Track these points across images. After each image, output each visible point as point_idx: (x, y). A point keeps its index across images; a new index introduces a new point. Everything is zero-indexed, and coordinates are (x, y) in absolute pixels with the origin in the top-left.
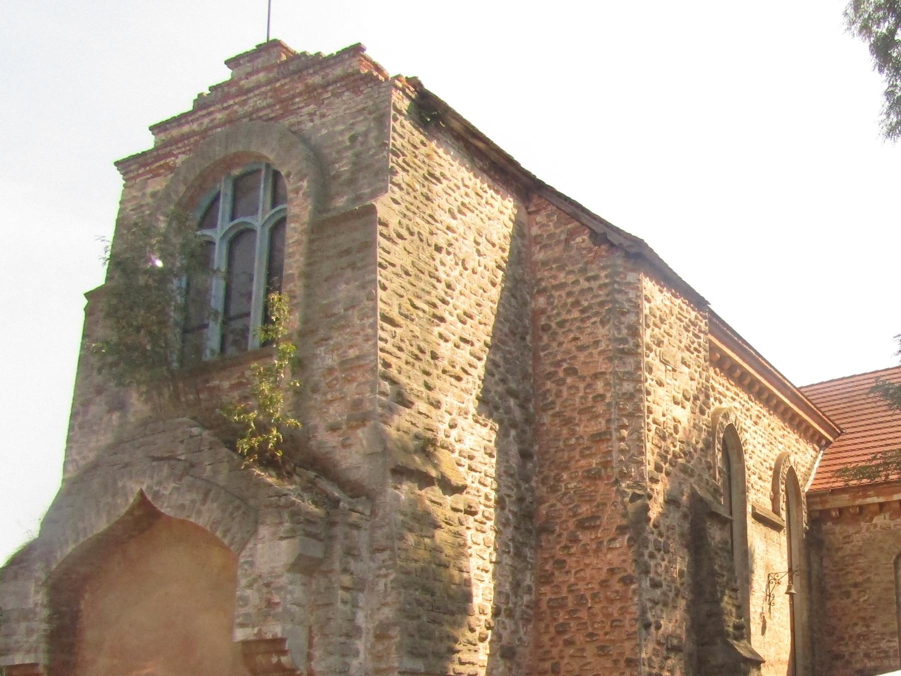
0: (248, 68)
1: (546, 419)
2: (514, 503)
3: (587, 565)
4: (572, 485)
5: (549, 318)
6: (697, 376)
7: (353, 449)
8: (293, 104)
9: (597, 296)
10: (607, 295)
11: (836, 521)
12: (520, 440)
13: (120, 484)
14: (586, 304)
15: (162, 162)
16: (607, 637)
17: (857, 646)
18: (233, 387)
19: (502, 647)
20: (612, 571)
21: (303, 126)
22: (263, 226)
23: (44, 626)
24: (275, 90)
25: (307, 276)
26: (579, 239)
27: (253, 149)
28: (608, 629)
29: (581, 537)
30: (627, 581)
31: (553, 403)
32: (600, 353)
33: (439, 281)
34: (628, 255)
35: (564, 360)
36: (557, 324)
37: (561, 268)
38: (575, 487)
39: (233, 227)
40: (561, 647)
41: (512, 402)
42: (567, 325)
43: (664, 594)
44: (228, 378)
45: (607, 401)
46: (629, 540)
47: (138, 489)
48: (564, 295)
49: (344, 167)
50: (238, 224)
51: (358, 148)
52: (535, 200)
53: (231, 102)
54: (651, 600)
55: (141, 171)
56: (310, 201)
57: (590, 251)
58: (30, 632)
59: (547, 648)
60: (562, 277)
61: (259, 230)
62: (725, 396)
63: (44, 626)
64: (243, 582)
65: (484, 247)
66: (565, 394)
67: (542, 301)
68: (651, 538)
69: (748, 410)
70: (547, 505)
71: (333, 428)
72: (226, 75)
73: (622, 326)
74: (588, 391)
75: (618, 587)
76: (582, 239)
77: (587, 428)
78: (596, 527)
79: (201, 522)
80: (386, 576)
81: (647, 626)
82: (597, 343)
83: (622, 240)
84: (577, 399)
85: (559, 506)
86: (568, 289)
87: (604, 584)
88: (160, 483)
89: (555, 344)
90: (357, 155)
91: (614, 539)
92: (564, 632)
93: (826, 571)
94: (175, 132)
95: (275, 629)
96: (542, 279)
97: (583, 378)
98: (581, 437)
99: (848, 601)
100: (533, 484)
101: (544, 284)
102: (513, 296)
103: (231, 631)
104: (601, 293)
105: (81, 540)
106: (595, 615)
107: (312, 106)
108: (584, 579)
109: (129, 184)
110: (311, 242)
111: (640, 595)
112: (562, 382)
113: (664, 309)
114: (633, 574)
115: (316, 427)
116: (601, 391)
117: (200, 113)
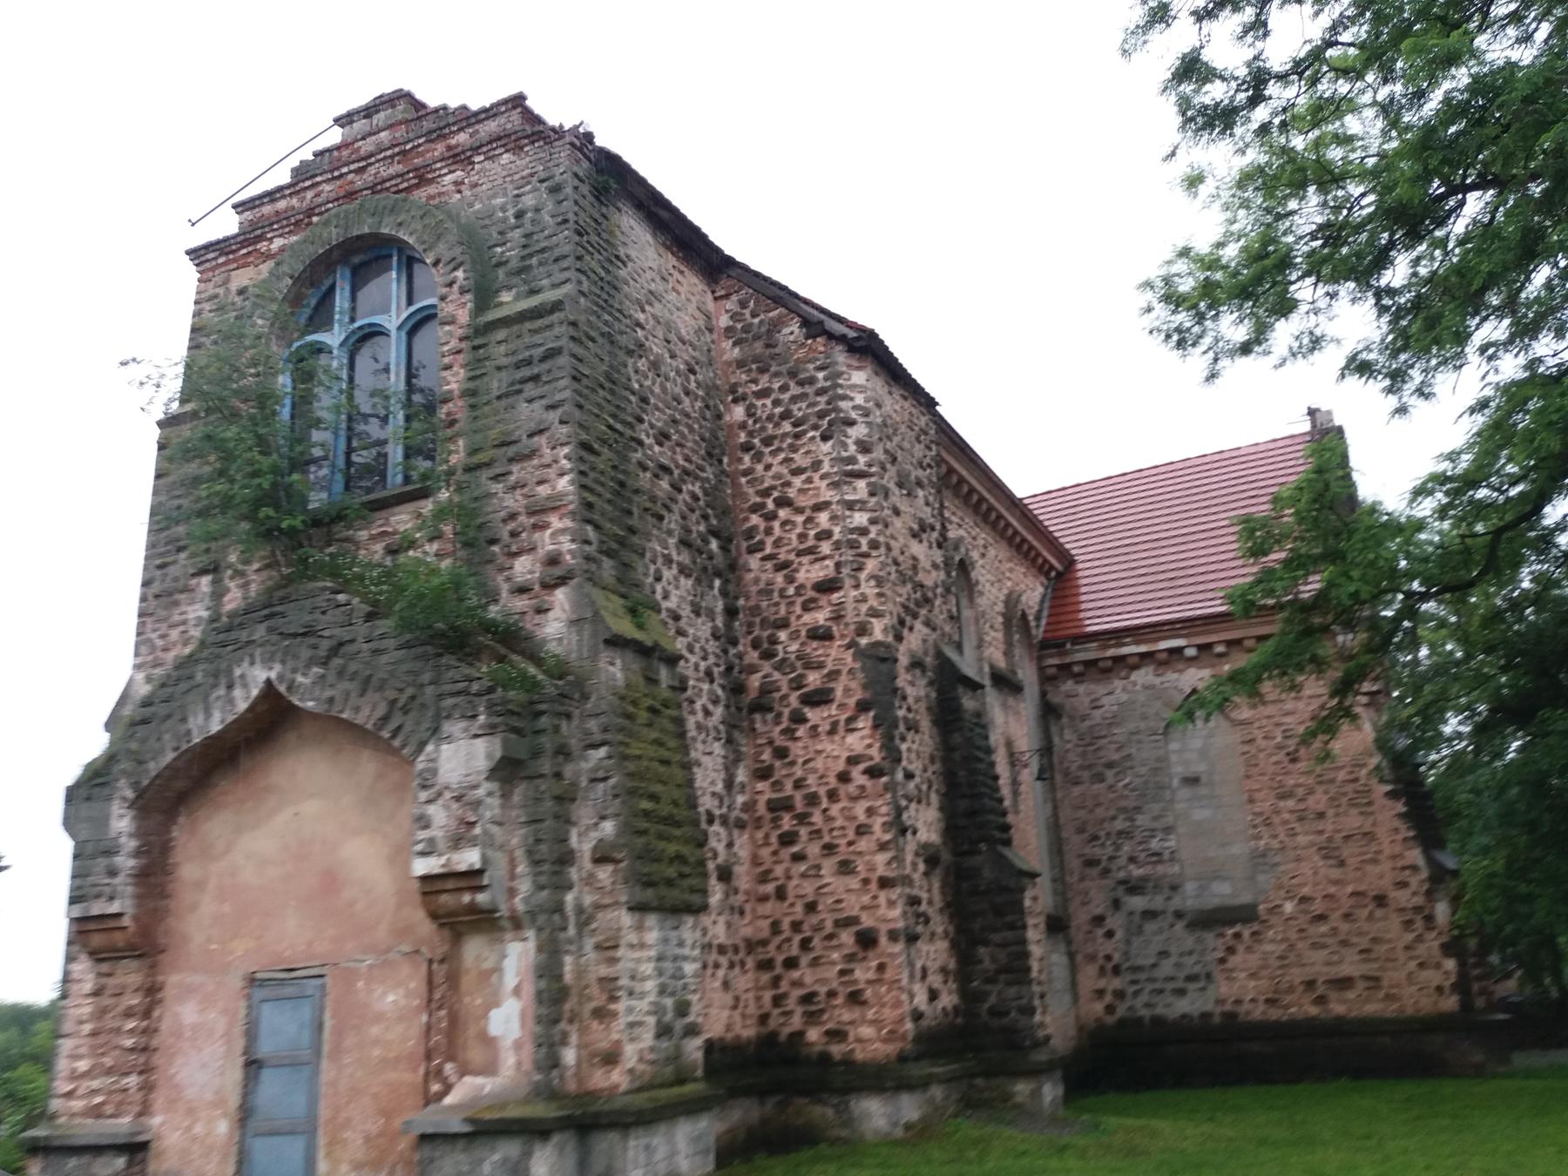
0: (360, 125)
3: (819, 752)
7: (551, 615)
10: (828, 403)
11: (1079, 678)
13: (238, 672)
17: (1118, 847)
23: (132, 862)
26: (786, 331)
28: (851, 835)
37: (762, 371)
39: (353, 332)
42: (776, 444)
43: (918, 787)
46: (875, 718)
50: (360, 328)
51: (528, 227)
53: (345, 170)
61: (393, 333)
63: (132, 862)
65: (678, 348)
66: (777, 531)
67: (739, 412)
70: (760, 675)
71: (522, 590)
72: (335, 136)
73: (849, 441)
76: (792, 330)
77: (811, 573)
78: (829, 701)
82: (817, 465)
84: (794, 537)
85: (776, 675)
86: (773, 396)
87: (844, 777)
89: (760, 467)
94: (267, 209)
95: (470, 858)
97: (800, 511)
100: (740, 648)
106: (832, 819)
107: (459, 173)
111: (894, 791)
117: (302, 185)
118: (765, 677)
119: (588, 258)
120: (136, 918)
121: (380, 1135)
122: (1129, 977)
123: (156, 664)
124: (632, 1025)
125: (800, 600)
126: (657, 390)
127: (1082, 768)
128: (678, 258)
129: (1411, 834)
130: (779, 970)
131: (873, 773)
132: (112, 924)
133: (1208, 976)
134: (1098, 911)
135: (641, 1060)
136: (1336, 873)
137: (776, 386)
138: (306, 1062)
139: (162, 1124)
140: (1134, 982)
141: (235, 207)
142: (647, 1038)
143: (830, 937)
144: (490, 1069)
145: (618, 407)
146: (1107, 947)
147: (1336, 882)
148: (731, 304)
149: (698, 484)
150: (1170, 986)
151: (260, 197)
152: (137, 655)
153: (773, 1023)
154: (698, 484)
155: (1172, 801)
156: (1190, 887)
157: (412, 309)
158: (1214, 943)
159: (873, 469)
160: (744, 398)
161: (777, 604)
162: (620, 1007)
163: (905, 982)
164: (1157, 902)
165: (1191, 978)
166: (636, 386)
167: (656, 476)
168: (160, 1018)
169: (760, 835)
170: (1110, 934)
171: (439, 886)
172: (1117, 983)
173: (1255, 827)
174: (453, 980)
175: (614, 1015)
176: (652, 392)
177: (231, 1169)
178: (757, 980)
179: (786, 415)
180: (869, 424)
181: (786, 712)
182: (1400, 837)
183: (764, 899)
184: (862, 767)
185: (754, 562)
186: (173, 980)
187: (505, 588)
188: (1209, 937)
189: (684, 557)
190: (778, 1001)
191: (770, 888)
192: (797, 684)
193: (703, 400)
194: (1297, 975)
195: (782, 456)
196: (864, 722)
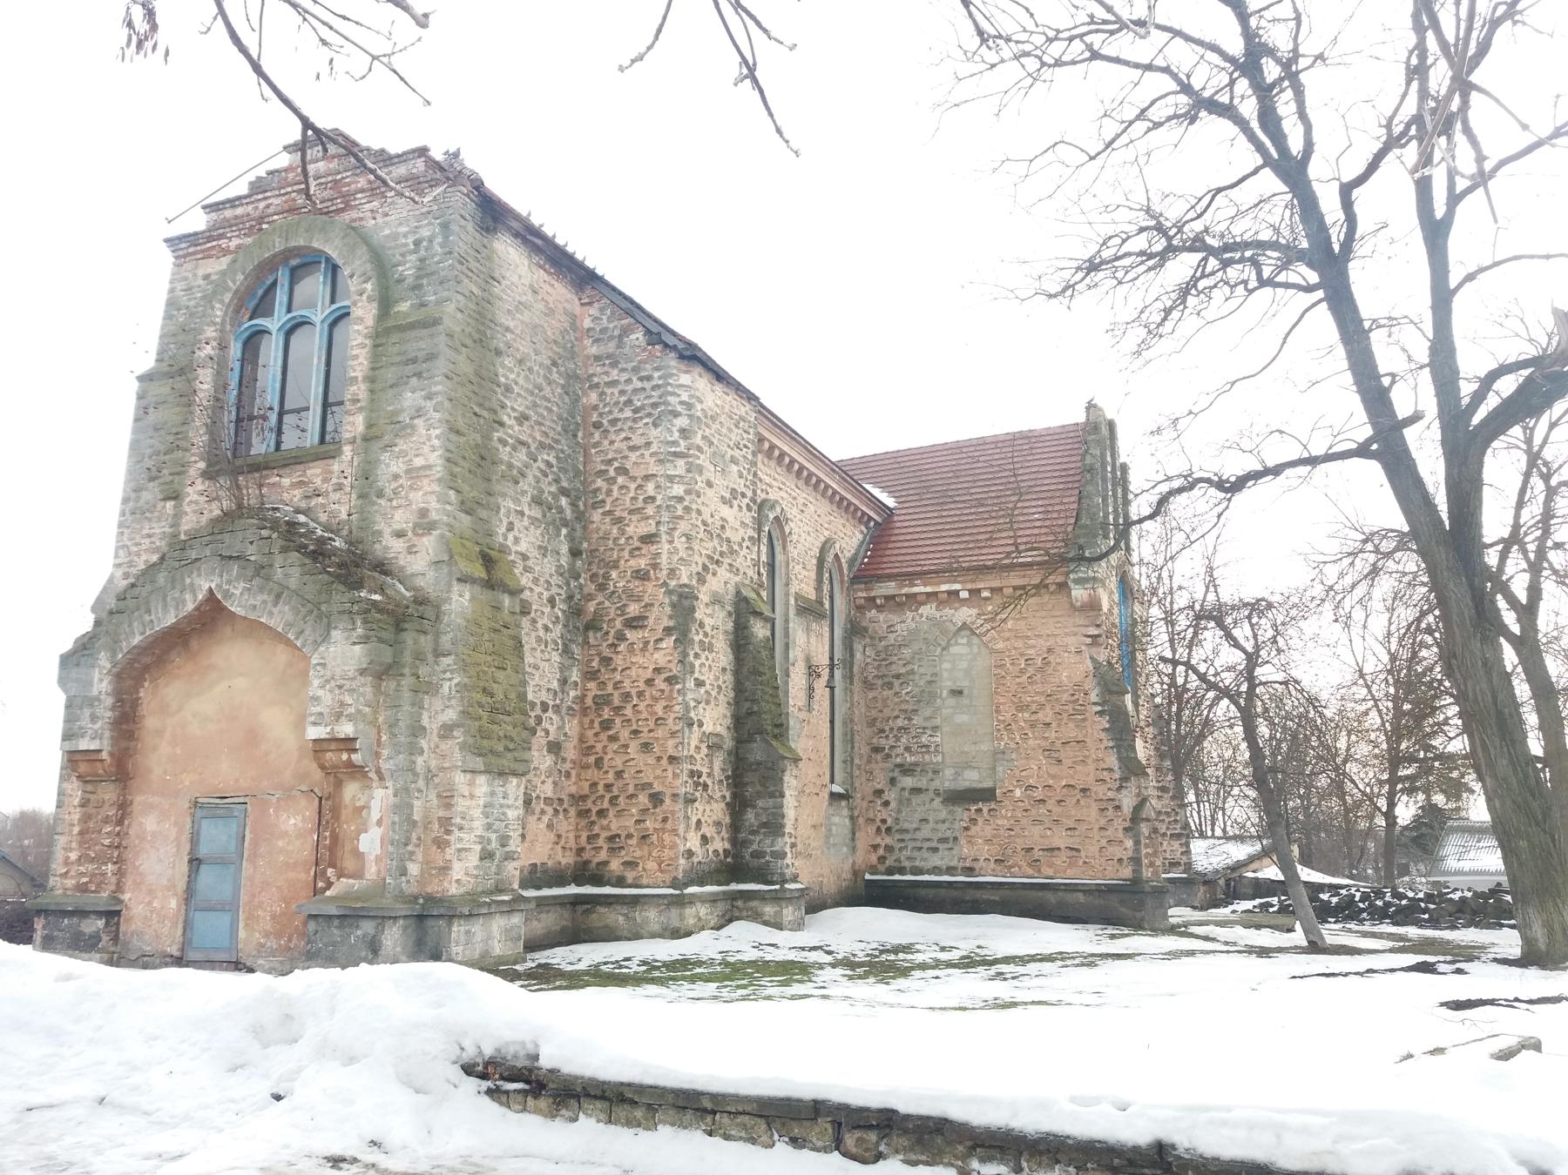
1: (596, 516)
2: (564, 601)
4: (621, 584)
5: (601, 415)
6: (745, 472)
8: (355, 199)
10: (660, 397)
11: (880, 608)
12: (571, 538)
13: (188, 581)
14: (639, 404)
15: (214, 243)
17: (898, 739)
18: (294, 485)
19: (549, 742)
22: (322, 322)
23: (109, 714)
24: (336, 182)
25: (371, 380)
26: (633, 337)
27: (315, 245)
28: (651, 724)
29: (628, 636)
30: (671, 680)
31: (603, 501)
32: (651, 455)
33: (499, 386)
35: (616, 459)
36: (609, 421)
37: (614, 365)
40: (605, 743)
41: (564, 501)
42: (619, 423)
44: (290, 475)
45: (658, 503)
49: (408, 270)
50: (294, 318)
51: (423, 252)
52: (588, 291)
53: (289, 189)
54: (695, 700)
56: (375, 305)
57: (644, 350)
58: (94, 718)
59: (591, 743)
61: (318, 325)
62: (771, 487)
63: (109, 714)
64: (316, 683)
66: (615, 494)
67: (594, 397)
68: (697, 638)
69: (795, 498)
71: (400, 534)
73: (674, 429)
75: (663, 686)
76: (638, 336)
77: (637, 528)
78: (643, 627)
79: (272, 623)
80: (450, 679)
81: (691, 725)
82: (648, 444)
84: (628, 500)
85: (607, 604)
86: (620, 387)
87: (650, 682)
88: (229, 582)
89: (606, 443)
90: (422, 260)
92: (609, 729)
94: (228, 213)
95: (346, 729)
97: (633, 479)
98: (631, 537)
99: (891, 692)
100: (582, 581)
101: (596, 380)
102: (567, 393)
105: (148, 633)
107: (375, 203)
111: (684, 695)
112: (612, 481)
113: (716, 409)
115: (380, 533)
118: (599, 604)
119: (466, 280)
120: (111, 754)
121: (283, 914)
122: (898, 836)
123: (131, 564)
125: (628, 548)
126: (521, 381)
127: (877, 677)
128: (550, 274)
129: (1111, 744)
130: (594, 818)
131: (669, 680)
132: (93, 757)
133: (955, 839)
134: (879, 787)
136: (1054, 770)
137: (622, 379)
138: (230, 861)
140: (903, 840)
141: (204, 207)
142: (473, 860)
143: (631, 797)
145: (484, 397)
146: (884, 814)
147: (1053, 777)
148: (593, 311)
149: (553, 454)
150: (927, 845)
151: (223, 203)
152: (116, 557)
153: (586, 856)
154: (553, 454)
155: (939, 709)
156: (948, 772)
157: (334, 307)
158: (962, 814)
160: (597, 385)
162: (452, 838)
163: (681, 831)
164: (922, 782)
165: (943, 840)
166: (503, 380)
167: (514, 449)
169: (586, 721)
170: (886, 804)
171: (325, 746)
172: (888, 840)
174: (336, 812)
175: (448, 843)
176: (516, 383)
181: (612, 632)
182: (1102, 747)
183: (586, 767)
184: (664, 676)
186: (139, 800)
187: (387, 531)
188: (959, 810)
189: (536, 512)
190: (592, 838)
191: (592, 759)
193: (563, 387)
194: (1020, 844)
195: (623, 435)
196: (669, 643)
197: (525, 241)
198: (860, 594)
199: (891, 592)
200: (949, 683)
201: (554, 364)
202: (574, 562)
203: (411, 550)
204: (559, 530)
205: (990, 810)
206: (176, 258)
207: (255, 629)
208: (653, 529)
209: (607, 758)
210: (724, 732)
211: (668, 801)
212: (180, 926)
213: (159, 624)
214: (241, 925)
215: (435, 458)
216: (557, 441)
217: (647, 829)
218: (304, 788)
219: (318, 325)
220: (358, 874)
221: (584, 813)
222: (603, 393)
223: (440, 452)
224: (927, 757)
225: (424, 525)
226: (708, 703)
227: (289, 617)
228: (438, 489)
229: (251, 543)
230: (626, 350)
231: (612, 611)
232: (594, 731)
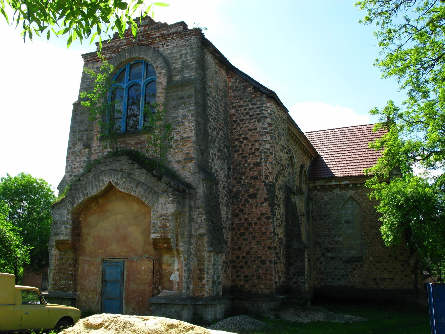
5: (237, 118)
9: (256, 111)
10: (260, 111)
11: (318, 190)
12: (228, 164)
14: (252, 114)
16: (261, 238)
20: (262, 214)
21: (160, 49)
22: (143, 84)
25: (165, 105)
26: (249, 89)
28: (261, 235)
29: (250, 201)
31: (238, 150)
32: (257, 133)
34: (268, 97)
35: (243, 134)
36: (240, 120)
37: (241, 99)
38: (248, 182)
42: (244, 121)
47: (108, 181)
48: (243, 110)
51: (183, 59)
53: (129, 37)
55: (91, 59)
60: (242, 103)
63: (71, 227)
66: (243, 147)
67: (233, 111)
70: (236, 188)
74: (252, 146)
75: (265, 220)
76: (250, 89)
82: (256, 129)
83: (267, 91)
84: (248, 150)
85: (241, 188)
87: (259, 219)
89: (239, 128)
90: (183, 62)
91: (263, 203)
93: (314, 210)
96: (233, 103)
97: (251, 141)
101: (234, 105)
103: (150, 236)
104: (257, 110)
108: (251, 217)
109: (86, 63)
110: (167, 93)
111: (274, 224)
112: (242, 142)
114: (271, 216)
115: (171, 161)
116: (258, 147)
118: (238, 189)
120: (72, 241)
124: (207, 281)
130: (238, 269)
131: (267, 218)
135: (209, 289)
137: (245, 105)
139: (80, 294)
140: (327, 276)
143: (253, 261)
144: (171, 288)
148: (233, 80)
154: (223, 132)
159: (272, 132)
160: (235, 107)
161: (242, 168)
165: (343, 276)
168: (78, 268)
169: (234, 232)
170: (321, 263)
173: (364, 236)
175: (203, 278)
177: (1, 303)
178: (232, 271)
179: (247, 113)
180: (271, 118)
181: (243, 200)
183: (235, 250)
185: (236, 156)
187: (174, 161)
190: (238, 276)
191: (237, 247)
192: (247, 191)
196: (266, 204)
197: (214, 55)
198: (311, 185)
199: (323, 184)
200: (344, 218)
201: (222, 99)
202: (229, 173)
203: (183, 168)
204: (224, 160)
205: (360, 265)
206: (85, 61)
207: (126, 197)
208: (258, 160)
209: (243, 247)
210: (283, 238)
211: (268, 263)
212: (100, 305)
213: (90, 194)
214: (124, 305)
215: (192, 134)
216: (223, 127)
217: (260, 273)
218: (147, 256)
219: (142, 85)
220: (171, 288)
221: (233, 267)
222: (237, 110)
223: (194, 132)
224: (336, 246)
225: (188, 159)
226: (279, 227)
227: (142, 193)
228: (194, 145)
229: (126, 165)
230: (246, 94)
231: (243, 192)
232: (237, 237)
